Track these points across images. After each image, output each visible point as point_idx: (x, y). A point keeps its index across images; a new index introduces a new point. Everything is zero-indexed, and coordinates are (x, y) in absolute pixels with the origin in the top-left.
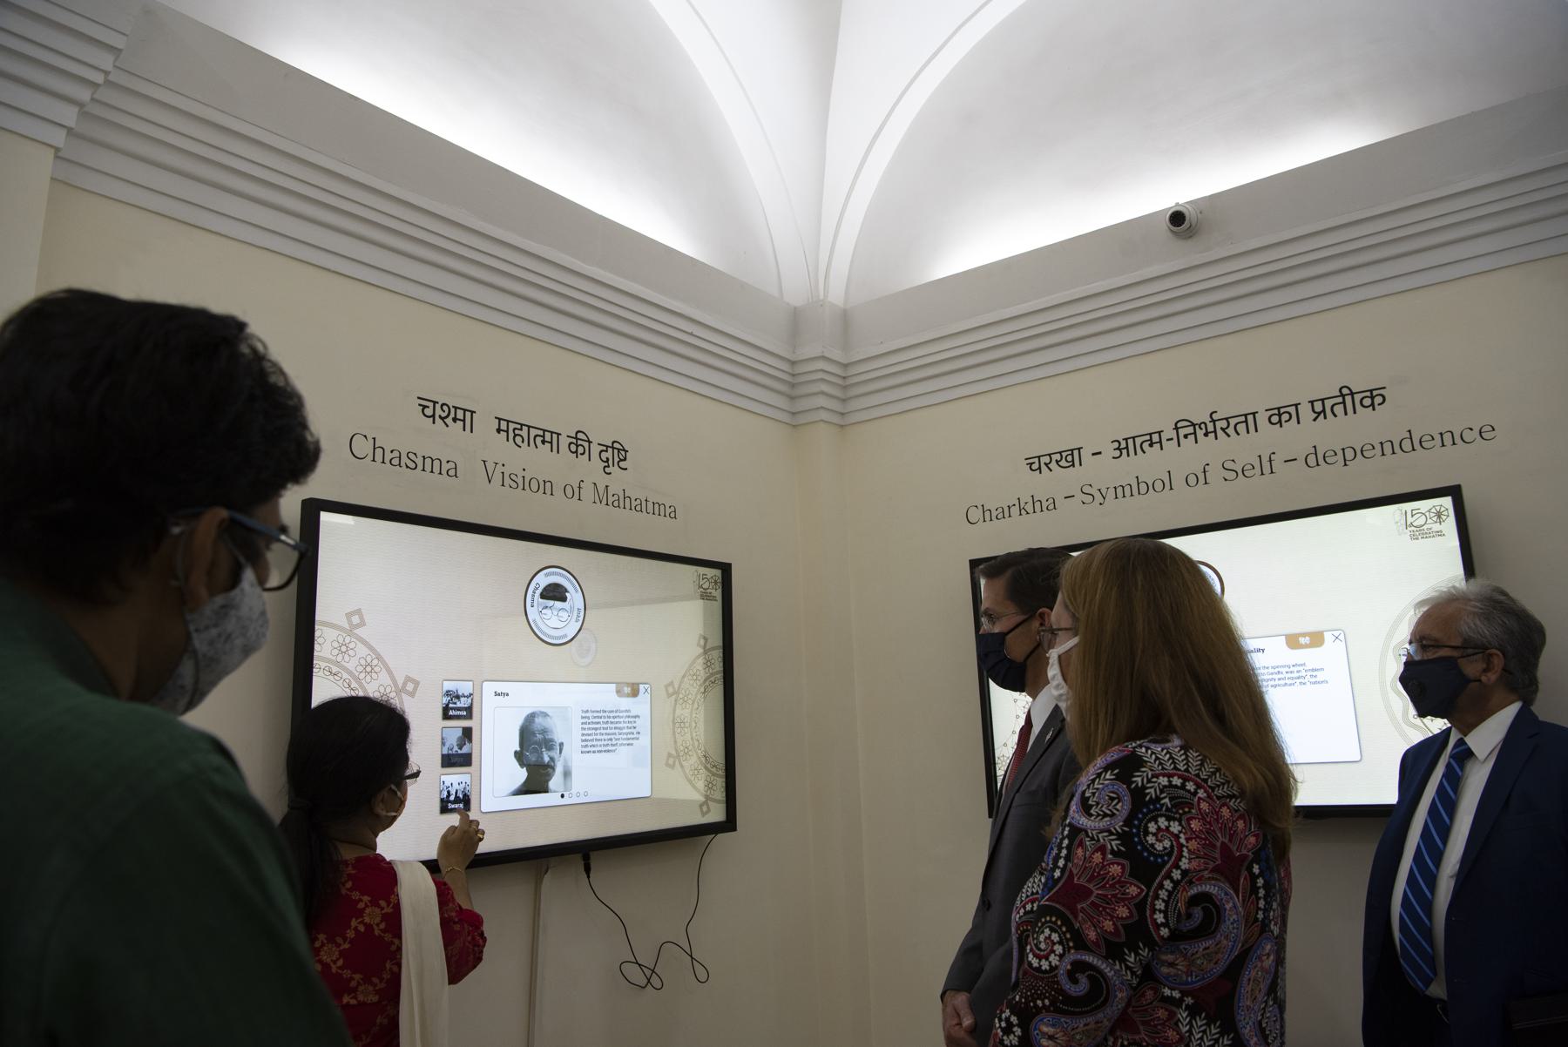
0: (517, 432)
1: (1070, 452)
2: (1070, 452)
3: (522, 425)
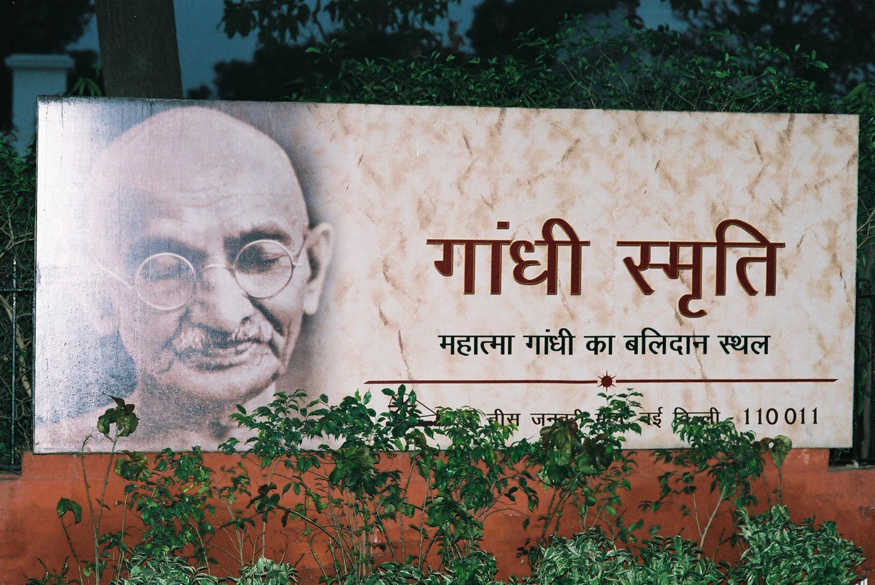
1: (633, 339)
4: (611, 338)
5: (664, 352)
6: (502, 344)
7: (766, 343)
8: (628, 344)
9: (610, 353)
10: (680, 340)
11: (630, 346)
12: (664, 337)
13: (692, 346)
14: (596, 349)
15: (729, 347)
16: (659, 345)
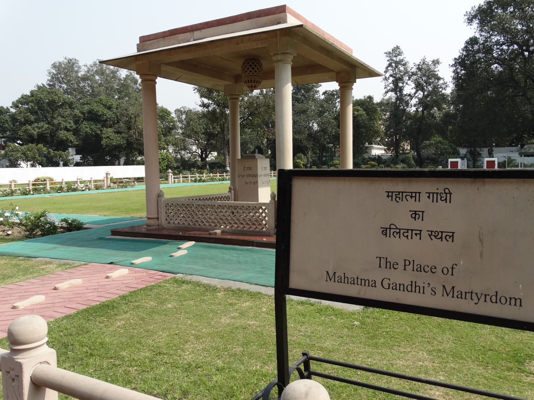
0: (397, 196)
1: (385, 229)
2: (385, 229)
3: (408, 230)
4: (423, 212)
5: (400, 237)
7: (453, 236)
9: (422, 220)
11: (383, 233)
12: (400, 229)
13: (414, 235)
14: (415, 218)
15: (432, 237)
16: (397, 233)
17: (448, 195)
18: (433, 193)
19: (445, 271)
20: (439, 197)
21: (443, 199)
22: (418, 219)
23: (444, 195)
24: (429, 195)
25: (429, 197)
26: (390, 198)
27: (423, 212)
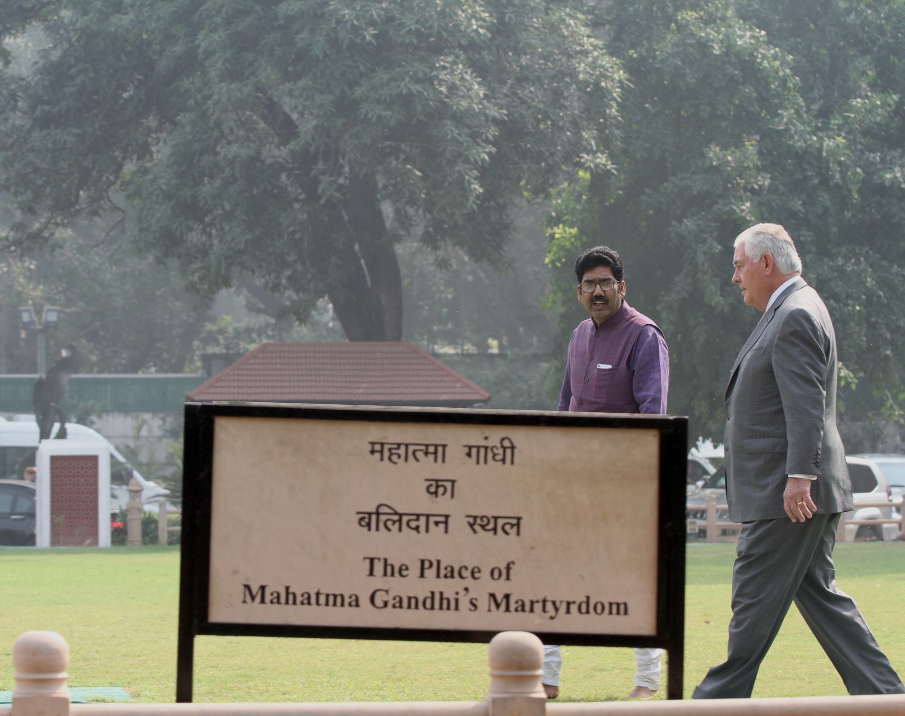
0: (394, 451)
6: (435, 453)
7: (518, 525)
8: (362, 519)
10: (417, 520)
12: (401, 515)
13: (432, 525)
14: (436, 493)
15: (477, 527)
16: (394, 522)
17: (508, 452)
18: (478, 447)
19: (496, 574)
20: (490, 455)
21: (498, 458)
22: (444, 494)
23: (500, 451)
24: (470, 450)
25: (469, 455)
26: (378, 455)
27: (453, 482)
